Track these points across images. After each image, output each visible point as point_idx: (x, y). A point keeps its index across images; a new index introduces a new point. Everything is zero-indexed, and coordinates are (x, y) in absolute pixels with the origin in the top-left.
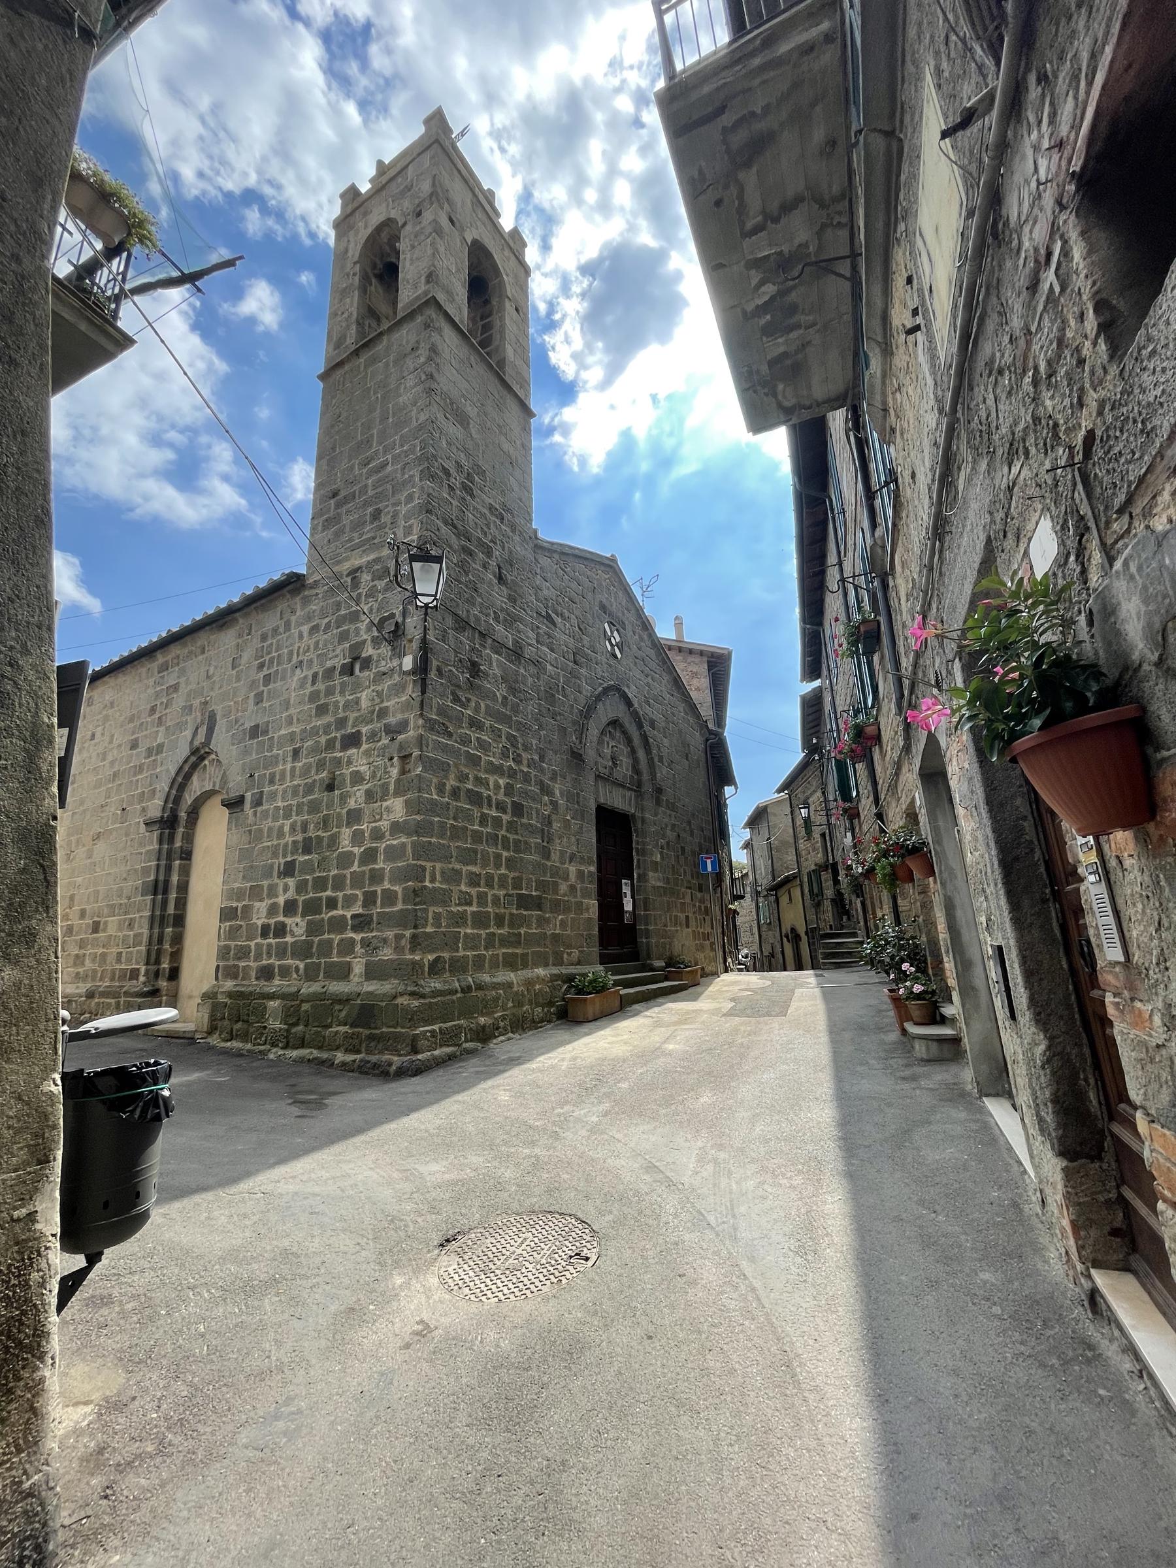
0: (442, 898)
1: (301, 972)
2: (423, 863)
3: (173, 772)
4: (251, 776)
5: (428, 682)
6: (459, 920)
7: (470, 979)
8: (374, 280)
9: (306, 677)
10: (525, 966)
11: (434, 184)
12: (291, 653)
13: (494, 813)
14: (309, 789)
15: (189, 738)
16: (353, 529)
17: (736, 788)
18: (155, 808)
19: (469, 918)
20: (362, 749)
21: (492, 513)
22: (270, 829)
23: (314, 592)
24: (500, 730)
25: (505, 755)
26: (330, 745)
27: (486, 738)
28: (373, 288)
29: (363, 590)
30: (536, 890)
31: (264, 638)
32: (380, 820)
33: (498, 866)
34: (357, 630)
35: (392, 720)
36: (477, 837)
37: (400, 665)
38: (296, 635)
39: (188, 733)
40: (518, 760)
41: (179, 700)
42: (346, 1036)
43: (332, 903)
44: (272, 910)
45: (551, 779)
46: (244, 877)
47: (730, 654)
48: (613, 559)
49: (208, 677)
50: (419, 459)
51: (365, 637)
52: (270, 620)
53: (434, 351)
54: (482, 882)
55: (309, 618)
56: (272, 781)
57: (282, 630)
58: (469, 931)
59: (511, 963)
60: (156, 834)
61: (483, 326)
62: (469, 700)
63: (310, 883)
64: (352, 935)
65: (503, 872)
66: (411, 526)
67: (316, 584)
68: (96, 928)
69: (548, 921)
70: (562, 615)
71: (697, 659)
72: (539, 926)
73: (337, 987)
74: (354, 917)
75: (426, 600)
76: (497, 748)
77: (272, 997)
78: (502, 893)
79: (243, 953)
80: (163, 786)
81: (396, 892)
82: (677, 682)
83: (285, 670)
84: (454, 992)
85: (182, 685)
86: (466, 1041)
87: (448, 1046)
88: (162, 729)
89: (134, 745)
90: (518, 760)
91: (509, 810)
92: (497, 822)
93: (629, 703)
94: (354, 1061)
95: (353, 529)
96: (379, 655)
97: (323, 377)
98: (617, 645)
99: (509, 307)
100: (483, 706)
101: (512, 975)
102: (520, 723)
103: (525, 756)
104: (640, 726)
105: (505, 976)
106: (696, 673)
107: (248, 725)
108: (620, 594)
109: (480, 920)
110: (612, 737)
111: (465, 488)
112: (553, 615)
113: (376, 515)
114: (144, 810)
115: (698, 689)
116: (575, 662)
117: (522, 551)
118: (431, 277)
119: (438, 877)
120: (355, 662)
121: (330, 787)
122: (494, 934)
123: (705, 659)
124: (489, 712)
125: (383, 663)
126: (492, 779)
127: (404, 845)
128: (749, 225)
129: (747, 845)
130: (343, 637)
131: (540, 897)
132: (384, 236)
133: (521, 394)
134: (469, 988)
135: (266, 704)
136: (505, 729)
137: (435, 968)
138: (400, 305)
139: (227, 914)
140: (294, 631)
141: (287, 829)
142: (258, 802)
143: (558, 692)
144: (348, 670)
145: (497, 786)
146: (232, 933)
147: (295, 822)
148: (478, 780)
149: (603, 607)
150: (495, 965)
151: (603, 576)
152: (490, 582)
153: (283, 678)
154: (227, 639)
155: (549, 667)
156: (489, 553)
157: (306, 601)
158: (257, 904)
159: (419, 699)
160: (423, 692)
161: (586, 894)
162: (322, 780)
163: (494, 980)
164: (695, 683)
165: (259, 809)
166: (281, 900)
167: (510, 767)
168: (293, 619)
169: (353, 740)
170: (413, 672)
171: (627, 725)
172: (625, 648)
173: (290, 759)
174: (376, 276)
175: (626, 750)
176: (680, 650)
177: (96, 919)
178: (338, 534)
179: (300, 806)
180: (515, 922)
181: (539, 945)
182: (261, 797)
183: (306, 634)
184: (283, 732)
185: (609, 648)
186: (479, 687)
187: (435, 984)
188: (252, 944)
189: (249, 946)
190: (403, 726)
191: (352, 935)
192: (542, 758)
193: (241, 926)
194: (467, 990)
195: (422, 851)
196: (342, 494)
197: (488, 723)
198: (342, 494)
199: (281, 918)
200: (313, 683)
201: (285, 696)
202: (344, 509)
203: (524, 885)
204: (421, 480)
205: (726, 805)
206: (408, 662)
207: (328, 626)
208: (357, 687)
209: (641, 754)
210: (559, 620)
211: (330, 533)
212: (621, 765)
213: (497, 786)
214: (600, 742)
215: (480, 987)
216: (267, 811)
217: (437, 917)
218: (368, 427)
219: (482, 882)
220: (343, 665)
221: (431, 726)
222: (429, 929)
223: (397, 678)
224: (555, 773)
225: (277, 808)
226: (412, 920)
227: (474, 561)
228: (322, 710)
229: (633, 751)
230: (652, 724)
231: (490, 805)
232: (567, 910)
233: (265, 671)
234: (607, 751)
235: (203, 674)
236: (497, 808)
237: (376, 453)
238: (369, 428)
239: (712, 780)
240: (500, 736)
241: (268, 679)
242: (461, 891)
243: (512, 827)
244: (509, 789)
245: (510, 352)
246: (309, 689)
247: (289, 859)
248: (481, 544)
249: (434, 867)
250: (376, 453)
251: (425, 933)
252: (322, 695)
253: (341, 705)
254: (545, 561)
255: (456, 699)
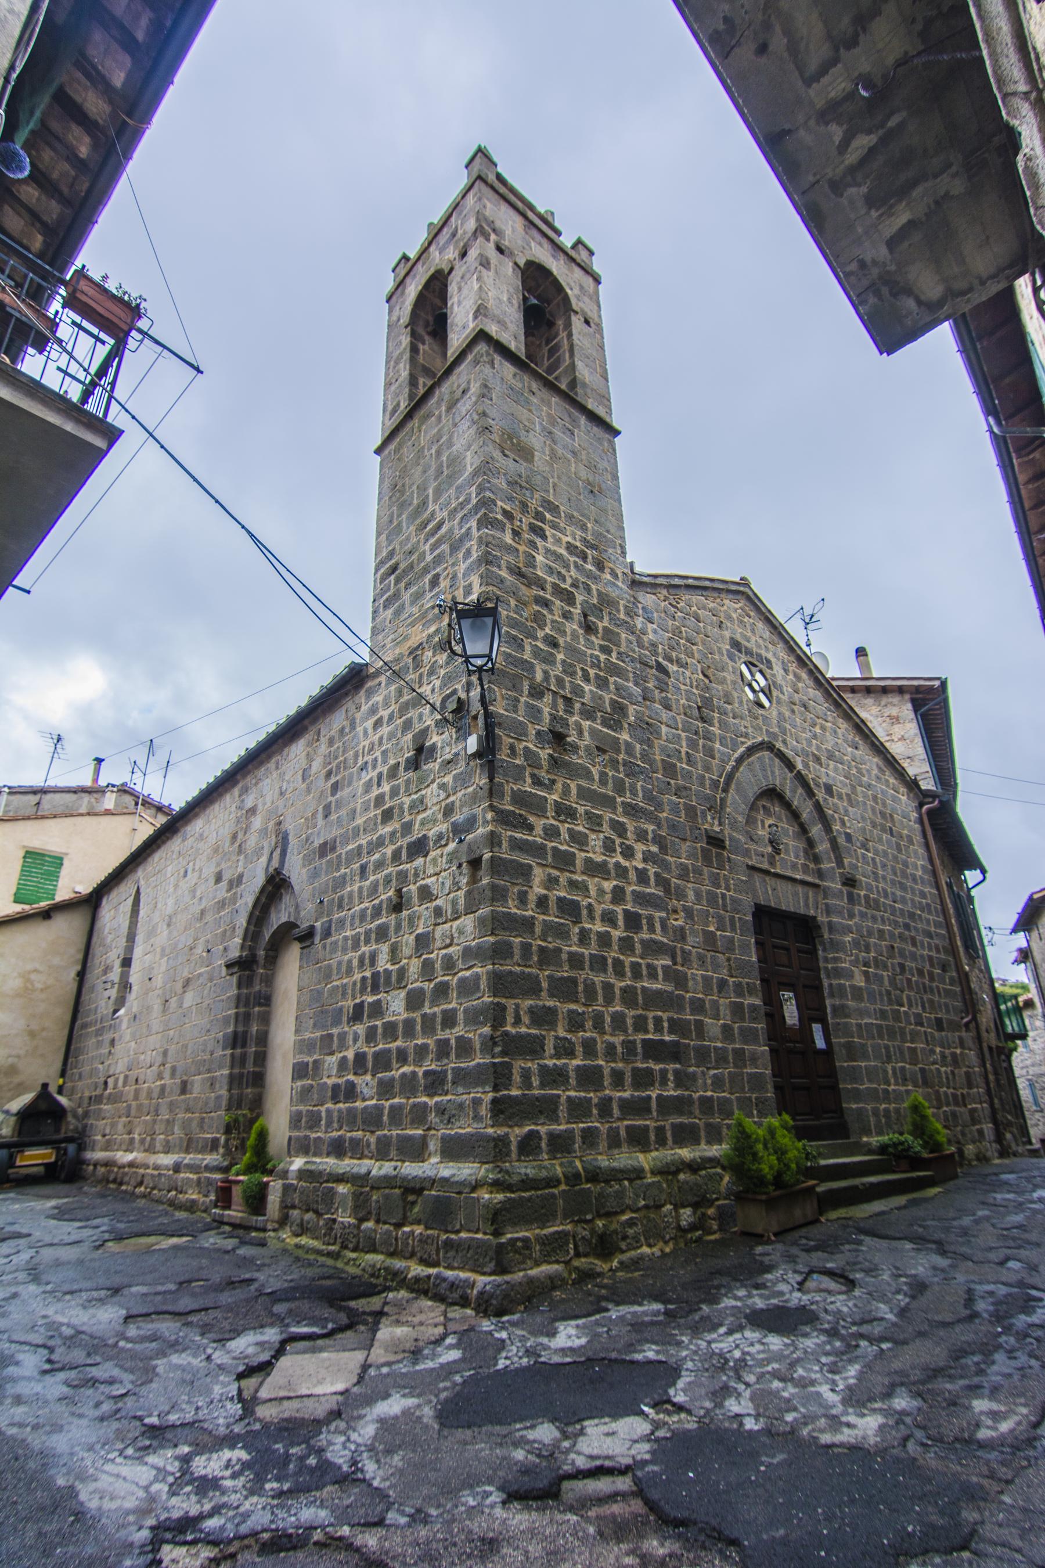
0: (532, 1047)
1: (373, 1147)
2: (503, 1001)
3: (250, 904)
4: (321, 902)
5: (497, 764)
6: (555, 1077)
7: (578, 1163)
8: (427, 338)
9: (371, 780)
10: (661, 1142)
11: (478, 220)
12: (356, 755)
13: (598, 927)
14: (377, 912)
15: (265, 865)
16: (413, 603)
17: (983, 872)
18: (235, 948)
19: (572, 1074)
20: (429, 858)
21: (571, 553)
22: (340, 963)
23: (377, 681)
24: (600, 817)
25: (609, 847)
26: (396, 856)
27: (580, 828)
28: (426, 347)
29: (425, 670)
30: (671, 1032)
31: (331, 742)
32: (450, 945)
33: (609, 1000)
34: (421, 716)
35: (458, 817)
36: (576, 961)
37: (465, 748)
38: (361, 734)
39: (264, 860)
40: (628, 853)
41: (257, 822)
42: (423, 1240)
43: (402, 1057)
44: (343, 1063)
45: (680, 877)
46: (315, 1025)
47: (944, 684)
48: (744, 582)
49: (281, 794)
50: (476, 508)
51: (428, 723)
52: (337, 720)
53: (486, 386)
54: (589, 1024)
55: (373, 711)
56: (340, 907)
57: (347, 730)
58: (572, 1093)
59: (639, 1139)
60: (235, 978)
61: (549, 351)
62: (553, 782)
63: (380, 1031)
64: (424, 1099)
65: (618, 1008)
66: (470, 585)
67: (378, 673)
68: (184, 1088)
69: (693, 1077)
70: (679, 662)
71: (895, 699)
72: (679, 1085)
73: (411, 1169)
74: (426, 1074)
75: (479, 662)
76: (595, 841)
77: (340, 1179)
78: (617, 1040)
79: (314, 1121)
80: (242, 921)
81: (470, 1039)
82: (879, 749)
83: (352, 774)
84: (551, 1182)
85: (260, 807)
86: (578, 1255)
87: (549, 1263)
88: (242, 857)
89: (218, 879)
90: (628, 853)
91: (621, 923)
92: (604, 940)
93: (790, 765)
94: (429, 1277)
95: (413, 603)
96: (443, 741)
97: (378, 451)
98: (762, 691)
99: (577, 322)
100: (573, 786)
101: (641, 1156)
102: (629, 805)
103: (639, 848)
104: (810, 793)
105: (625, 1158)
106: (897, 718)
107: (316, 844)
108: (760, 625)
109: (589, 1078)
110: (768, 812)
111: (533, 529)
112: (665, 663)
113: (435, 582)
114: (225, 949)
115: (902, 738)
116: (703, 720)
117: (620, 590)
118: (480, 311)
119: (526, 1019)
120: (421, 753)
121: (397, 907)
122: (610, 1099)
123: (907, 697)
124: (584, 794)
125: (447, 749)
126: (592, 884)
127: (477, 977)
128: (813, 65)
129: (1025, 956)
130: (407, 725)
131: (676, 1044)
132: (437, 285)
133: (601, 411)
134: (577, 1176)
135: (333, 817)
136: (608, 815)
137: (529, 1146)
138: (449, 353)
139: (300, 1071)
140: (360, 729)
141: (355, 963)
142: (327, 933)
143: (680, 760)
144: (414, 764)
145: (601, 892)
146: (304, 1094)
147: (364, 954)
148: (573, 884)
149: (736, 644)
150: (615, 1142)
151: (732, 606)
152: (574, 633)
153: (350, 784)
154: (298, 750)
155: (664, 729)
156: (570, 599)
157: (370, 693)
158: (328, 1058)
159: (487, 787)
160: (491, 779)
161: (749, 1036)
162: (390, 899)
163: (615, 1164)
164: (898, 730)
165: (329, 941)
166: (350, 1054)
167: (617, 865)
168: (358, 716)
169: (419, 848)
170: (478, 755)
171: (788, 794)
172: (775, 693)
173: (357, 878)
174: (429, 334)
175: (792, 829)
176: (868, 690)
177: (185, 1078)
178: (397, 613)
179: (368, 933)
180: (642, 1079)
181: (681, 1113)
182: (330, 927)
183: (370, 731)
184: (350, 847)
185: (751, 695)
186: (567, 765)
187: (526, 1169)
188: (323, 1109)
189: (319, 1112)
190: (471, 823)
191: (424, 1099)
192: (663, 848)
193: (312, 1086)
194: (573, 1178)
195: (500, 984)
196: (402, 566)
197: (581, 810)
198: (402, 566)
199: (351, 1077)
200: (379, 785)
201: (352, 806)
202: (403, 585)
203: (651, 1027)
204: (478, 529)
205: (971, 900)
206: (472, 743)
207: (391, 717)
208: (423, 782)
209: (816, 831)
210: (672, 668)
211: (389, 612)
212: (787, 852)
213: (601, 892)
214: (750, 821)
215: (594, 1175)
216: (336, 943)
217: (526, 1075)
218: (421, 488)
219: (589, 1024)
220: (407, 759)
221: (504, 818)
222: (515, 1092)
223: (461, 767)
224: (684, 868)
225: (346, 938)
226: (499, 1077)
227: (551, 611)
228: (387, 816)
229: (803, 830)
230: (829, 789)
231: (592, 917)
232: (722, 1059)
233: (333, 780)
234: (762, 833)
235: (277, 791)
236: (603, 920)
237: (433, 513)
238: (425, 489)
239: (937, 862)
240: (600, 825)
241: (335, 788)
242: (557, 1038)
243: (626, 944)
244: (618, 895)
245: (583, 371)
246: (375, 792)
247: (358, 1001)
248: (558, 591)
249: (517, 1006)
250: (433, 513)
251: (510, 1097)
252: (387, 798)
253: (406, 806)
254: (648, 599)
255: (537, 782)
